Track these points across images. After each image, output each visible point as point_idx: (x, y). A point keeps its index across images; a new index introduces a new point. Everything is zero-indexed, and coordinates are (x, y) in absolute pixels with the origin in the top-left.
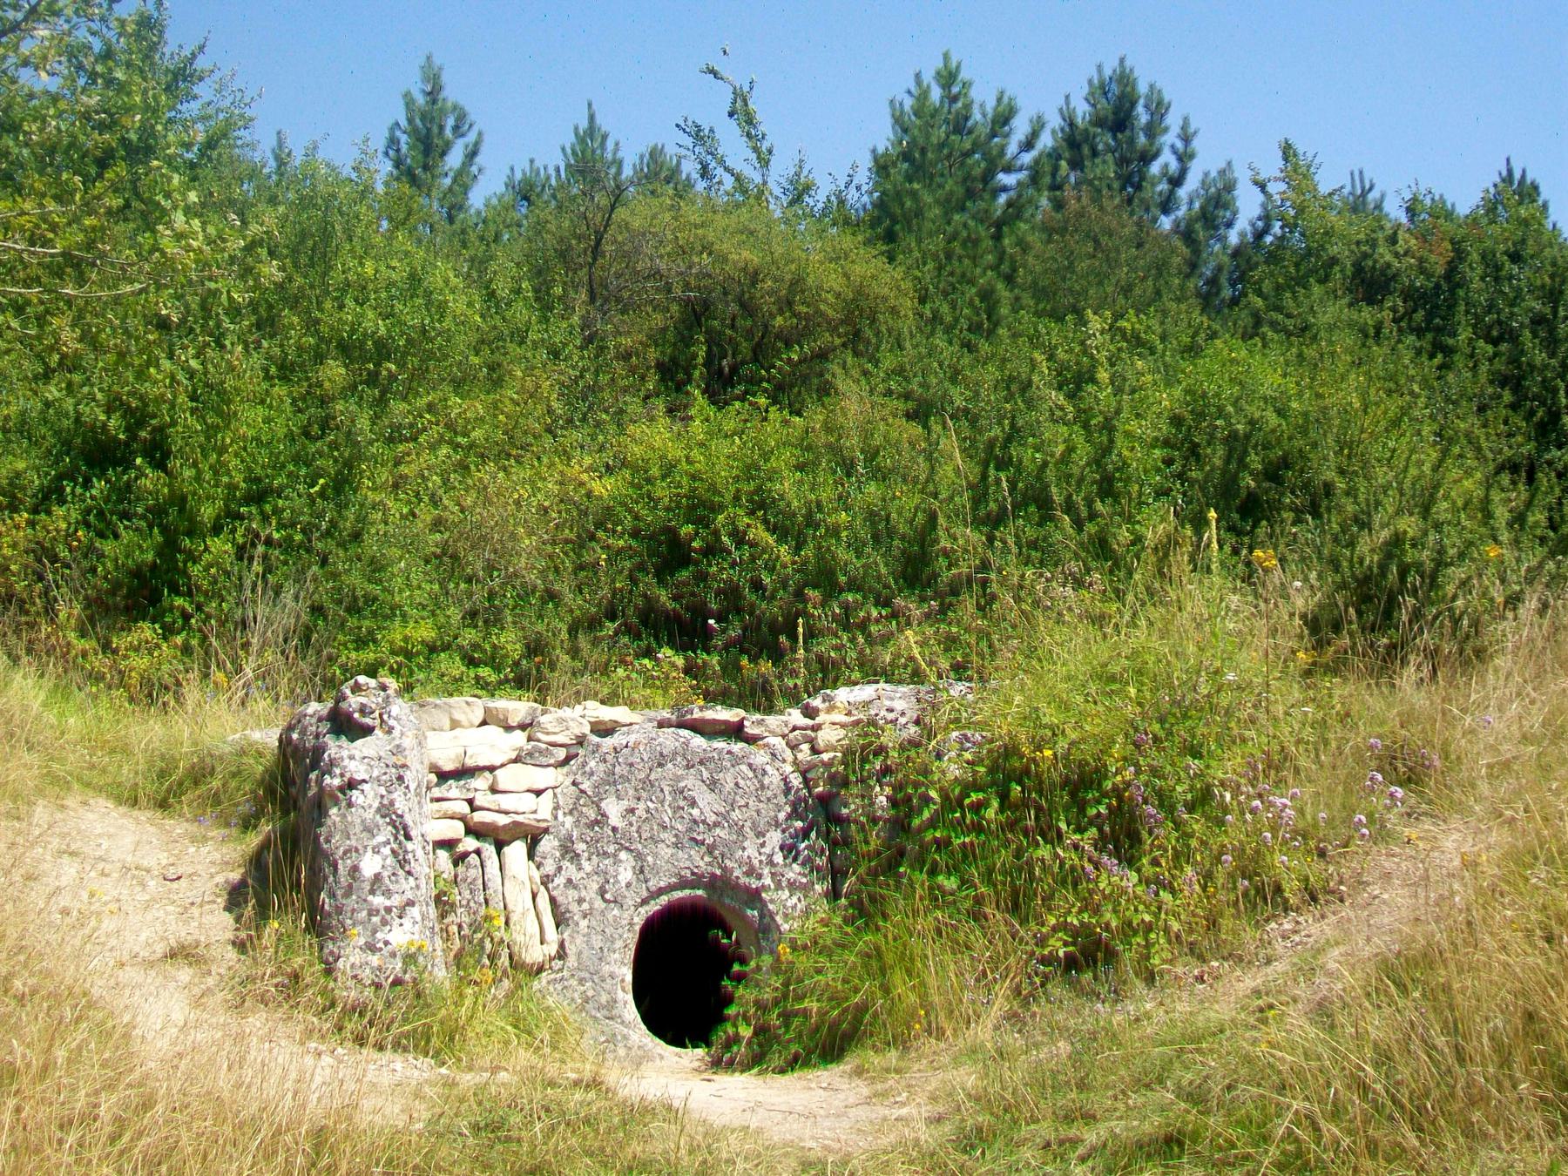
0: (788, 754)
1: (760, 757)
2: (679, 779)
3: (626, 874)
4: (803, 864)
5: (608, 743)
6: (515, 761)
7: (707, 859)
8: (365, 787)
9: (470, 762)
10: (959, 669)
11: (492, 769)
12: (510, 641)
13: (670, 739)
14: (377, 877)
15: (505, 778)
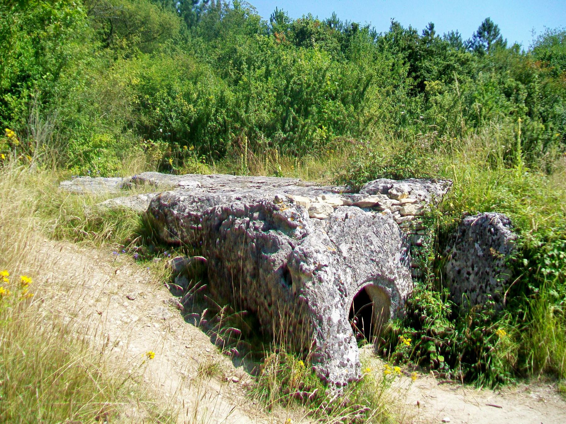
7: (377, 268)
8: (327, 269)
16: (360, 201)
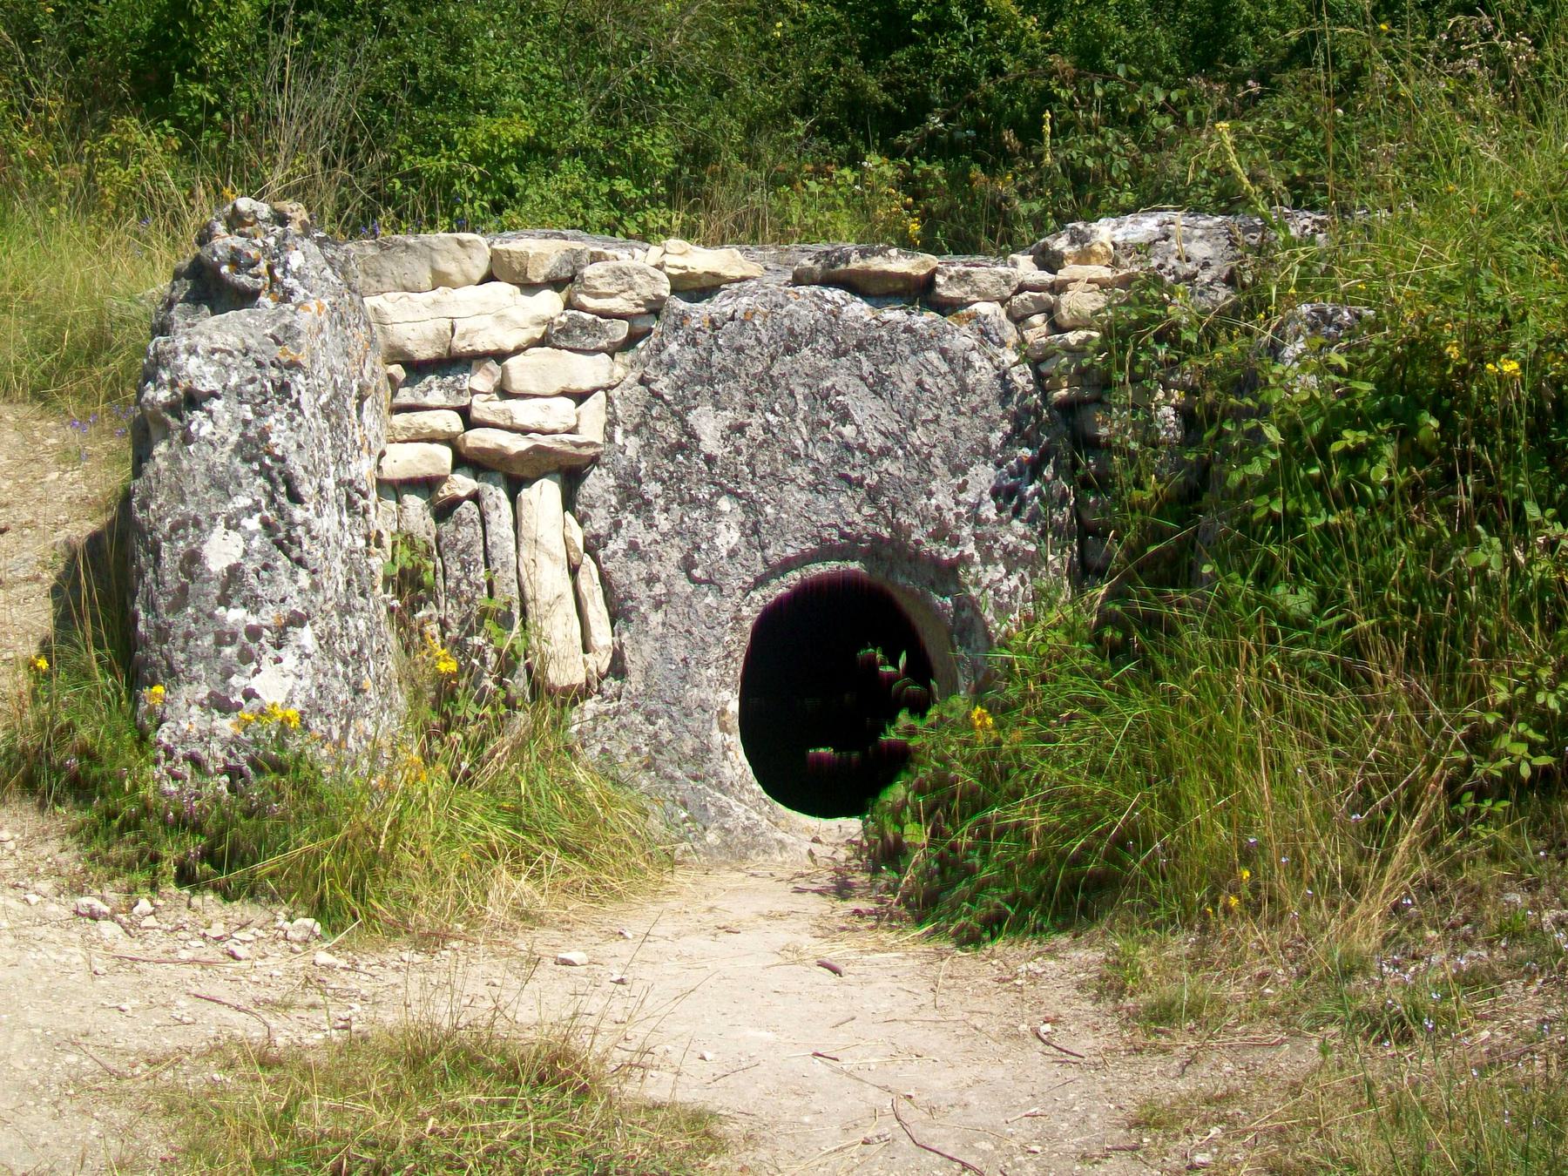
0: (1010, 332)
1: (962, 338)
2: (821, 374)
3: (729, 537)
4: (1031, 521)
5: (702, 311)
6: (542, 342)
7: (866, 510)
8: (217, 405)
9: (461, 345)
10: (1301, 194)
11: (500, 356)
12: (660, 146)
13: (805, 306)
14: (234, 572)
15: (521, 371)
16: (843, 267)
